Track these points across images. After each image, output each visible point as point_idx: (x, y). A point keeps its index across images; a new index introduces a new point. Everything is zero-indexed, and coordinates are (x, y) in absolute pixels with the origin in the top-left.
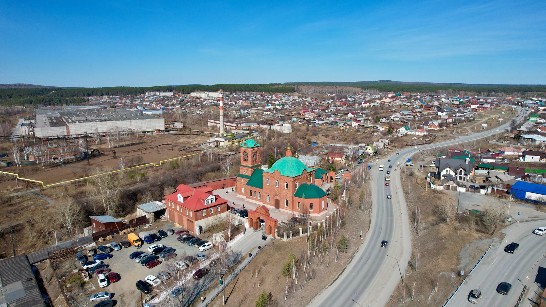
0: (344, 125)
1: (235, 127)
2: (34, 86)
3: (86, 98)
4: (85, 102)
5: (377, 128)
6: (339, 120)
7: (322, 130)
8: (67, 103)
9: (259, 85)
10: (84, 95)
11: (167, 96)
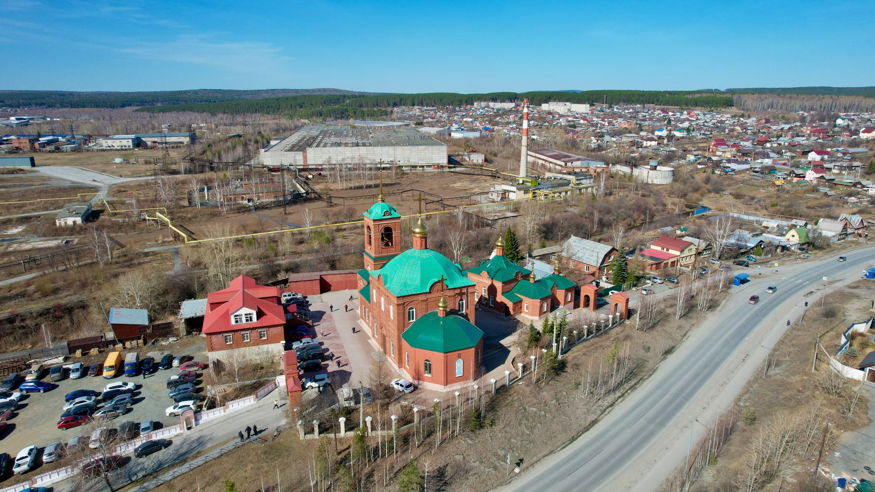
0: (789, 175)
1: (561, 166)
2: (341, 91)
3: (389, 109)
4: (385, 115)
5: (863, 186)
6: (784, 164)
7: (737, 182)
8: (363, 117)
9: (665, 92)
10: (389, 105)
11: (504, 109)
